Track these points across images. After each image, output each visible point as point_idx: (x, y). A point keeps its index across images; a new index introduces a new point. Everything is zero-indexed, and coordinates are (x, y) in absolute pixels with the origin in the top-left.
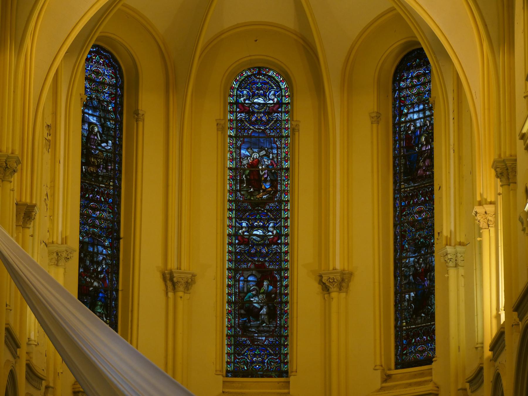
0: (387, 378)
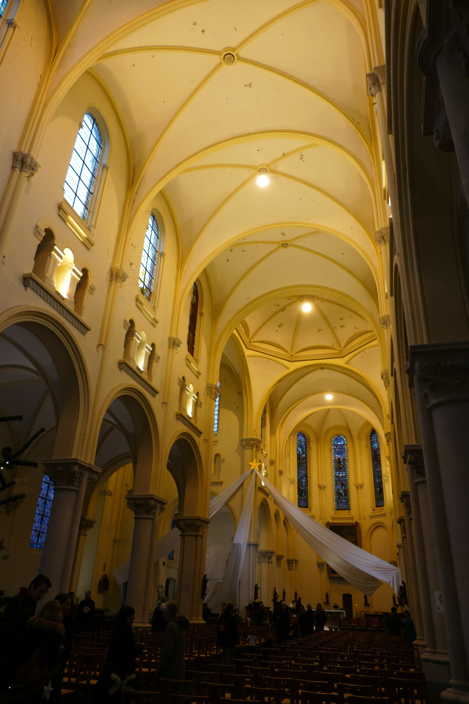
0: (374, 510)
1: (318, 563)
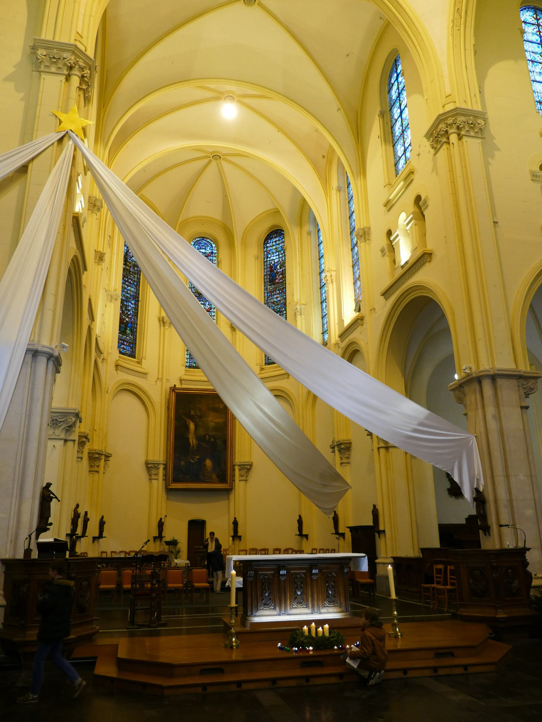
0: (262, 369)
1: (147, 464)
